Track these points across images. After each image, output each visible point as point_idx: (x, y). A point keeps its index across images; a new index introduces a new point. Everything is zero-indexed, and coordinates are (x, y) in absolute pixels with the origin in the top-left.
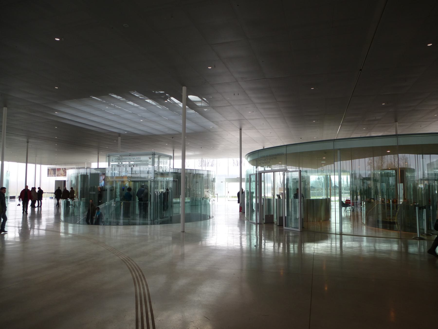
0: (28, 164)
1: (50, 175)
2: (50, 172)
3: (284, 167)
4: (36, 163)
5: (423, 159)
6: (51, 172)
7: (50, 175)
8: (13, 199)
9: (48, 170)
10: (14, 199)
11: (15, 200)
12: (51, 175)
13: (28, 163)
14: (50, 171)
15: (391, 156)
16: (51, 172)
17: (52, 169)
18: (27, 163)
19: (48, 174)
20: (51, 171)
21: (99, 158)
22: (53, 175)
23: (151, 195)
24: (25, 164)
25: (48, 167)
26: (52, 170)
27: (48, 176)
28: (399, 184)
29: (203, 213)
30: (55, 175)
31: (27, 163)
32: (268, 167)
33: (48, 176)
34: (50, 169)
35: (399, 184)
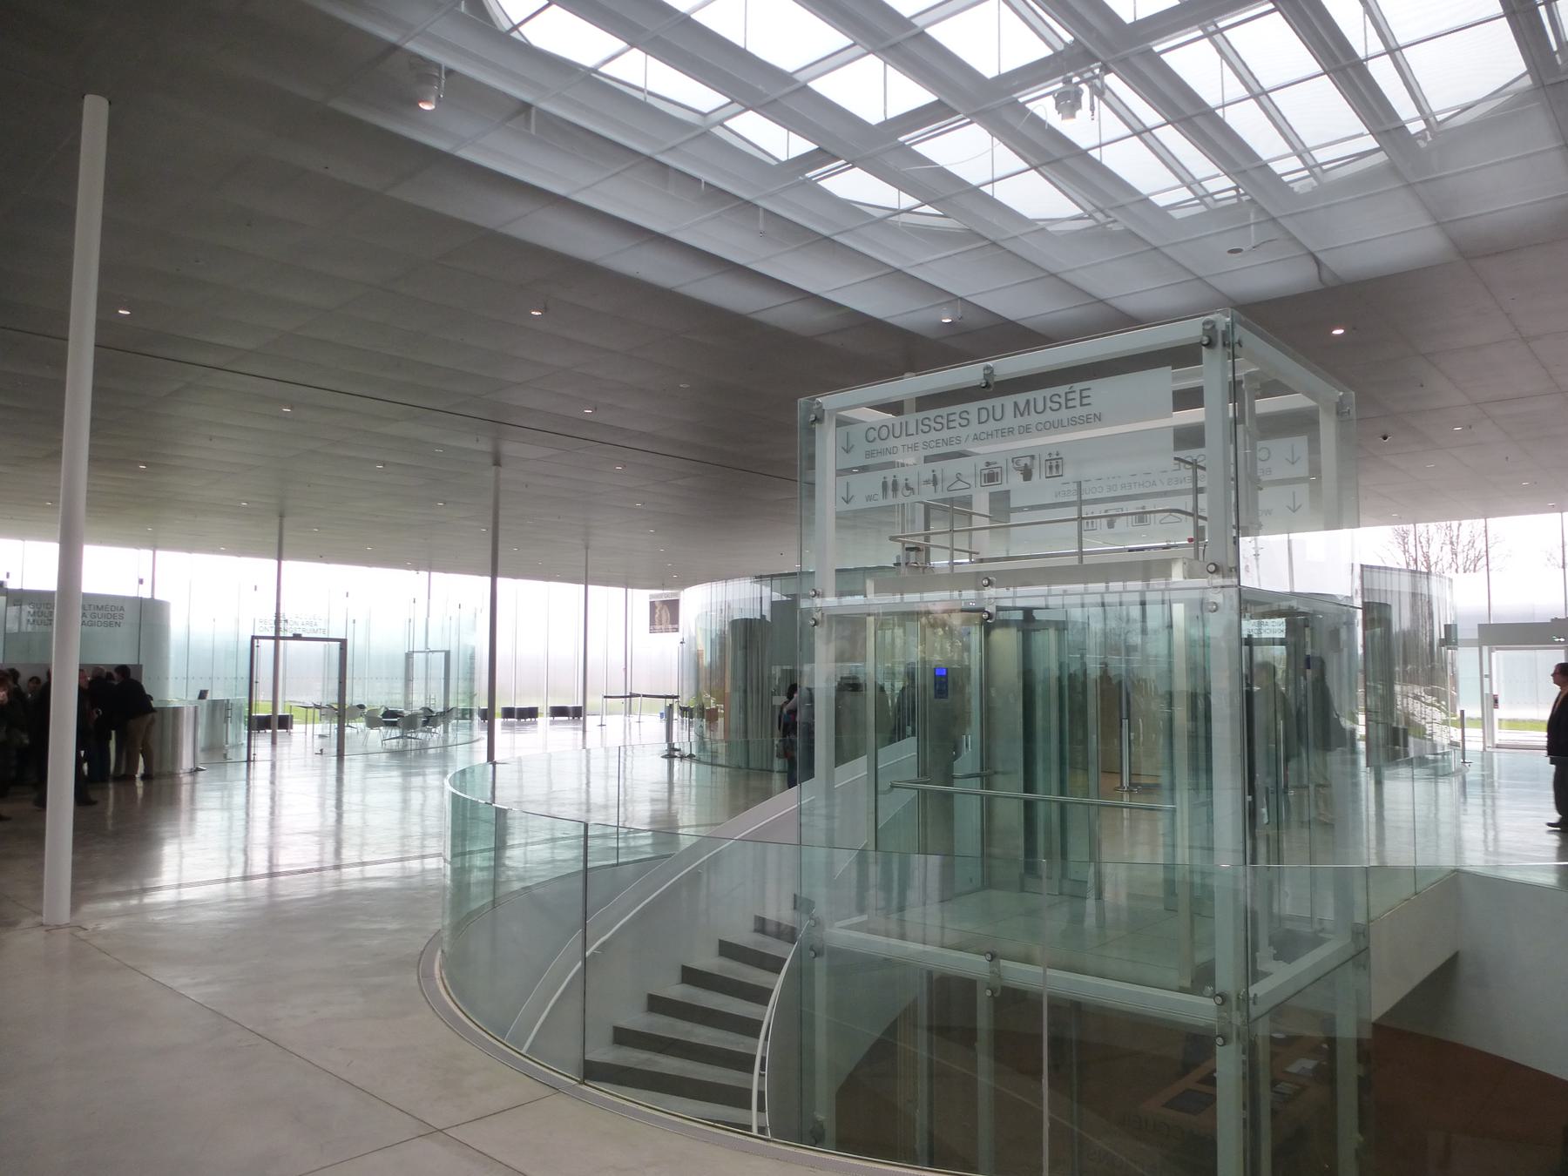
0: (500, 581)
1: (658, 627)
2: (657, 616)
3: (309, 710)
4: (586, 582)
5: (761, 598)
6: (660, 616)
7: (658, 627)
8: (529, 720)
9: (652, 604)
10: (533, 719)
11: (535, 723)
12: (663, 627)
13: (87, 544)
14: (657, 611)
15: (1260, 585)
16: (660, 616)
17: (664, 602)
18: (280, 558)
19: (652, 622)
20: (660, 611)
21: (286, 533)
22: (670, 626)
23: (779, 728)
24: (488, 580)
25: (651, 596)
26: (665, 606)
27: (652, 631)
28: (1020, 509)
29: (1268, 498)
30: (676, 626)
31: (280, 558)
32: (226, 702)
33: (652, 631)
34: (657, 604)
35: (1020, 509)
